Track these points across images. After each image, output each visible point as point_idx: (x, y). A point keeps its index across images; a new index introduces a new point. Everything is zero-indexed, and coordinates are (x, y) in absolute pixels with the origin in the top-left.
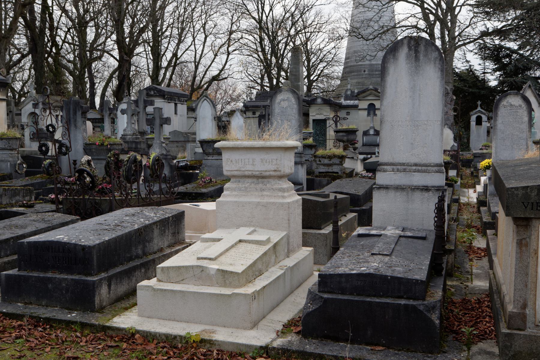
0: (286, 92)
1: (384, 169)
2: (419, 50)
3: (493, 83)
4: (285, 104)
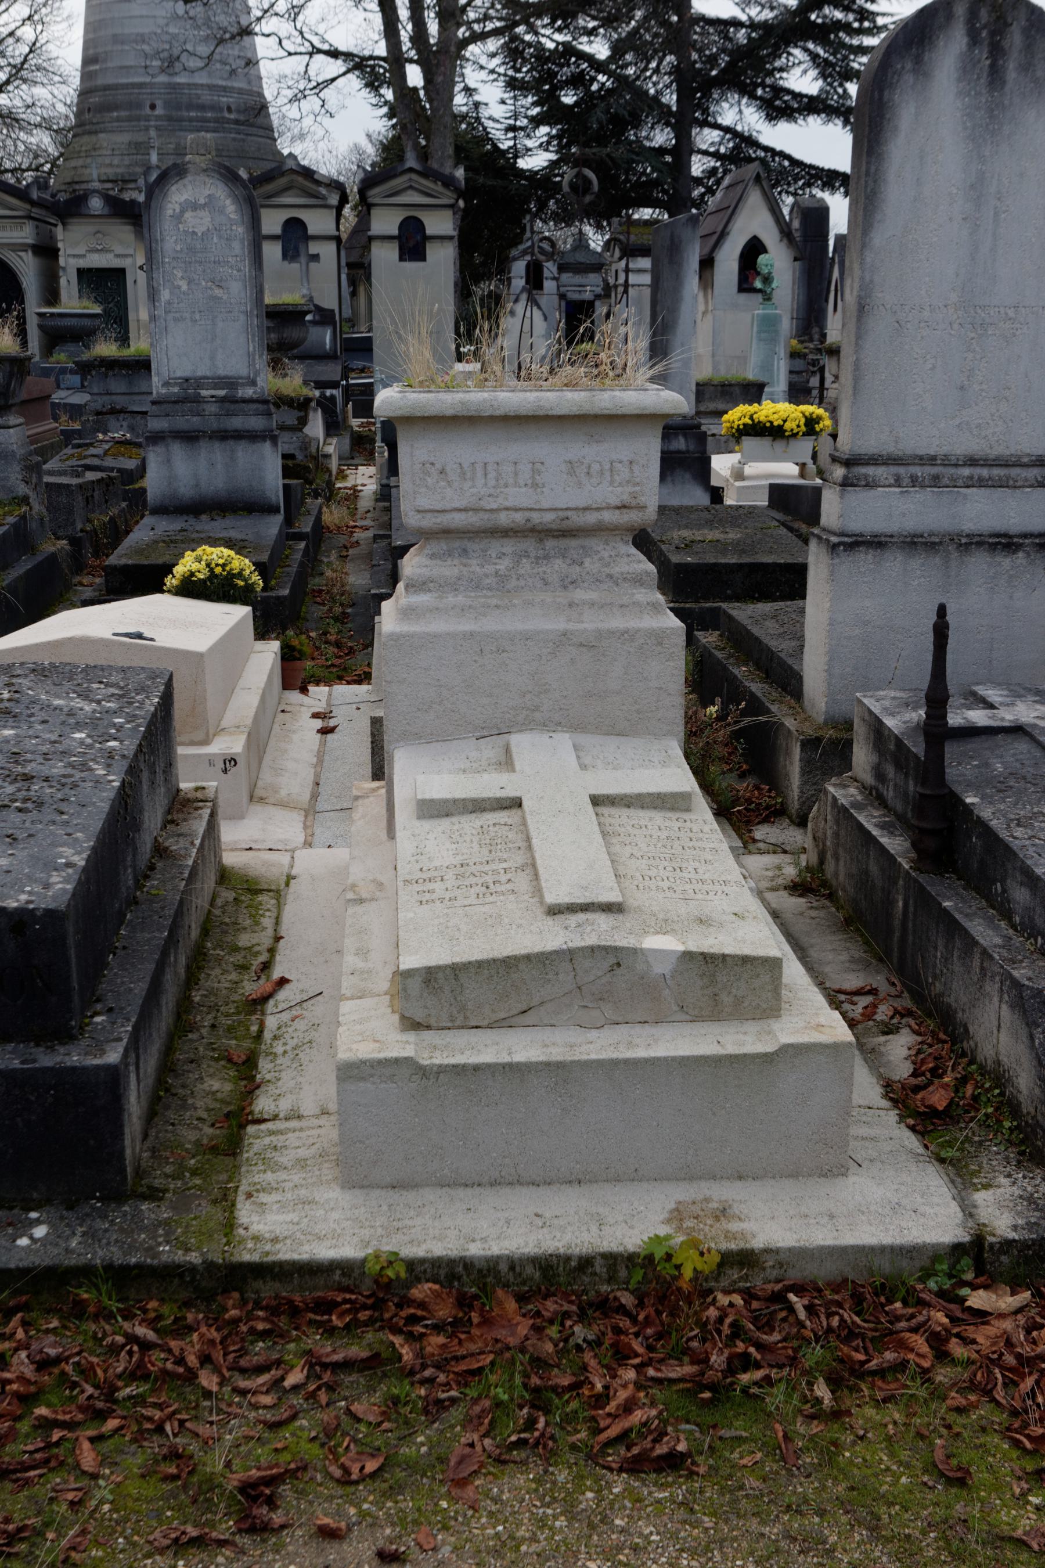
0: (202, 177)
1: (866, 476)
2: (1005, 43)
3: (535, 161)
4: (199, 222)
